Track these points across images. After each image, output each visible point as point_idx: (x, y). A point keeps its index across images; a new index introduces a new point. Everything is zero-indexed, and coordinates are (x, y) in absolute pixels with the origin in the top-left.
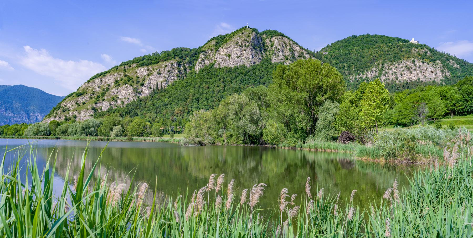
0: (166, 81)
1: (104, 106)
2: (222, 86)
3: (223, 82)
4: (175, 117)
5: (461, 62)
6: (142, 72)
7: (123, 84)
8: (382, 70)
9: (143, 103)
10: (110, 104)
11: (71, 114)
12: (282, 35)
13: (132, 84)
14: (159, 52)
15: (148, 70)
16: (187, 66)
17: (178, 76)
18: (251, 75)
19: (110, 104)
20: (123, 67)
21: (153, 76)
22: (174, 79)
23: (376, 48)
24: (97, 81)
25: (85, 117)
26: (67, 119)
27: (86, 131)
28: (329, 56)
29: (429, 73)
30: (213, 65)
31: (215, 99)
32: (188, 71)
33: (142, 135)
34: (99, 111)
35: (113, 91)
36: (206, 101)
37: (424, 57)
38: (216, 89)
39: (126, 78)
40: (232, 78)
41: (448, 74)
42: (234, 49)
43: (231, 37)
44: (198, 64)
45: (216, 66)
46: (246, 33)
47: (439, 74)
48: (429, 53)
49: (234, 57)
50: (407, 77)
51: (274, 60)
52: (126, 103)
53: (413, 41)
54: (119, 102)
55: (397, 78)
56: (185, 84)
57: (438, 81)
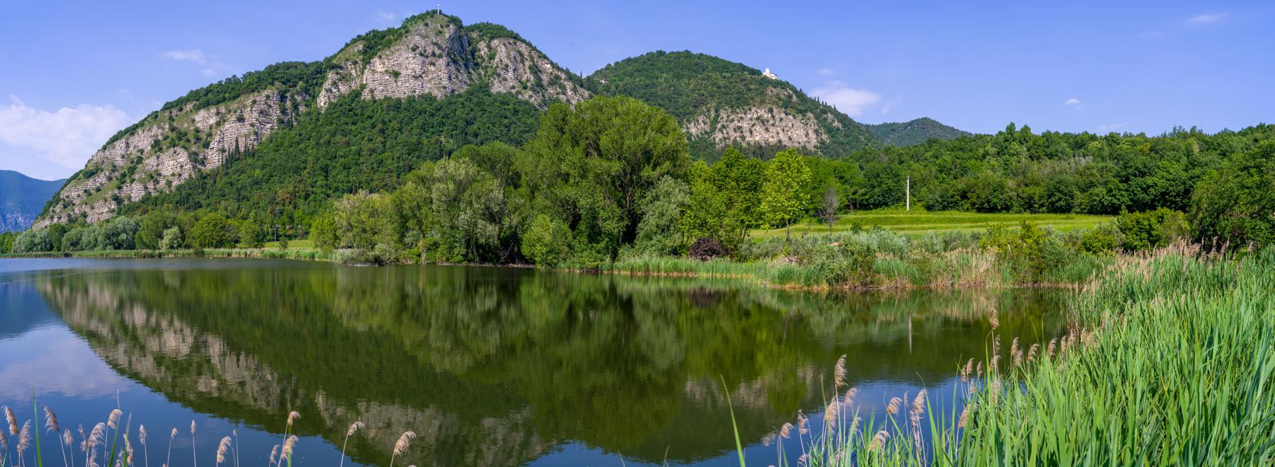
0: (256, 134)
1: (136, 192)
2: (380, 139)
3: (382, 131)
4: (278, 208)
5: (844, 119)
6: (204, 119)
7: (168, 148)
8: (715, 121)
9: (210, 181)
10: (146, 188)
11: (77, 211)
12: (516, 37)
13: (187, 145)
14: (240, 76)
15: (218, 113)
16: (299, 98)
17: (281, 121)
18: (446, 116)
19: (146, 188)
20: (167, 114)
21: (227, 126)
22: (272, 129)
23: (703, 79)
24: (120, 145)
25: (101, 212)
26: (72, 220)
27: (114, 240)
28: (613, 87)
29: (799, 133)
30: (357, 94)
31: (363, 167)
32: (302, 109)
33: (220, 244)
34: (126, 202)
35: (151, 162)
36: (345, 173)
37: (787, 105)
38: (366, 146)
39: (174, 135)
40: (401, 122)
41: (825, 137)
42: (408, 62)
43: (401, 35)
44: (323, 93)
45: (366, 95)
46: (435, 24)
47: (813, 136)
48: (795, 98)
49: (406, 75)
50: (759, 136)
51: (497, 88)
52: (175, 183)
53: (767, 73)
54: (163, 182)
55: (743, 138)
56: (297, 139)
57: (810, 147)
